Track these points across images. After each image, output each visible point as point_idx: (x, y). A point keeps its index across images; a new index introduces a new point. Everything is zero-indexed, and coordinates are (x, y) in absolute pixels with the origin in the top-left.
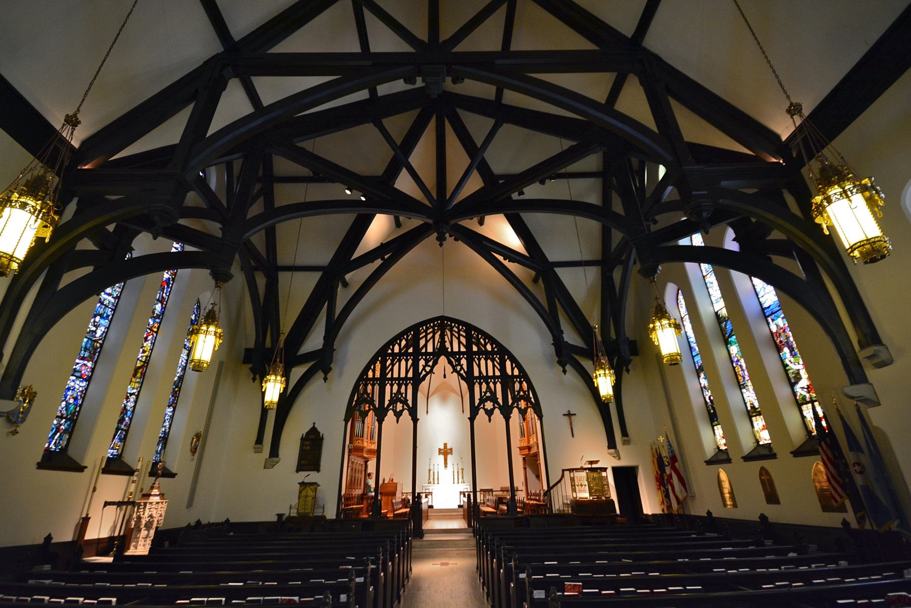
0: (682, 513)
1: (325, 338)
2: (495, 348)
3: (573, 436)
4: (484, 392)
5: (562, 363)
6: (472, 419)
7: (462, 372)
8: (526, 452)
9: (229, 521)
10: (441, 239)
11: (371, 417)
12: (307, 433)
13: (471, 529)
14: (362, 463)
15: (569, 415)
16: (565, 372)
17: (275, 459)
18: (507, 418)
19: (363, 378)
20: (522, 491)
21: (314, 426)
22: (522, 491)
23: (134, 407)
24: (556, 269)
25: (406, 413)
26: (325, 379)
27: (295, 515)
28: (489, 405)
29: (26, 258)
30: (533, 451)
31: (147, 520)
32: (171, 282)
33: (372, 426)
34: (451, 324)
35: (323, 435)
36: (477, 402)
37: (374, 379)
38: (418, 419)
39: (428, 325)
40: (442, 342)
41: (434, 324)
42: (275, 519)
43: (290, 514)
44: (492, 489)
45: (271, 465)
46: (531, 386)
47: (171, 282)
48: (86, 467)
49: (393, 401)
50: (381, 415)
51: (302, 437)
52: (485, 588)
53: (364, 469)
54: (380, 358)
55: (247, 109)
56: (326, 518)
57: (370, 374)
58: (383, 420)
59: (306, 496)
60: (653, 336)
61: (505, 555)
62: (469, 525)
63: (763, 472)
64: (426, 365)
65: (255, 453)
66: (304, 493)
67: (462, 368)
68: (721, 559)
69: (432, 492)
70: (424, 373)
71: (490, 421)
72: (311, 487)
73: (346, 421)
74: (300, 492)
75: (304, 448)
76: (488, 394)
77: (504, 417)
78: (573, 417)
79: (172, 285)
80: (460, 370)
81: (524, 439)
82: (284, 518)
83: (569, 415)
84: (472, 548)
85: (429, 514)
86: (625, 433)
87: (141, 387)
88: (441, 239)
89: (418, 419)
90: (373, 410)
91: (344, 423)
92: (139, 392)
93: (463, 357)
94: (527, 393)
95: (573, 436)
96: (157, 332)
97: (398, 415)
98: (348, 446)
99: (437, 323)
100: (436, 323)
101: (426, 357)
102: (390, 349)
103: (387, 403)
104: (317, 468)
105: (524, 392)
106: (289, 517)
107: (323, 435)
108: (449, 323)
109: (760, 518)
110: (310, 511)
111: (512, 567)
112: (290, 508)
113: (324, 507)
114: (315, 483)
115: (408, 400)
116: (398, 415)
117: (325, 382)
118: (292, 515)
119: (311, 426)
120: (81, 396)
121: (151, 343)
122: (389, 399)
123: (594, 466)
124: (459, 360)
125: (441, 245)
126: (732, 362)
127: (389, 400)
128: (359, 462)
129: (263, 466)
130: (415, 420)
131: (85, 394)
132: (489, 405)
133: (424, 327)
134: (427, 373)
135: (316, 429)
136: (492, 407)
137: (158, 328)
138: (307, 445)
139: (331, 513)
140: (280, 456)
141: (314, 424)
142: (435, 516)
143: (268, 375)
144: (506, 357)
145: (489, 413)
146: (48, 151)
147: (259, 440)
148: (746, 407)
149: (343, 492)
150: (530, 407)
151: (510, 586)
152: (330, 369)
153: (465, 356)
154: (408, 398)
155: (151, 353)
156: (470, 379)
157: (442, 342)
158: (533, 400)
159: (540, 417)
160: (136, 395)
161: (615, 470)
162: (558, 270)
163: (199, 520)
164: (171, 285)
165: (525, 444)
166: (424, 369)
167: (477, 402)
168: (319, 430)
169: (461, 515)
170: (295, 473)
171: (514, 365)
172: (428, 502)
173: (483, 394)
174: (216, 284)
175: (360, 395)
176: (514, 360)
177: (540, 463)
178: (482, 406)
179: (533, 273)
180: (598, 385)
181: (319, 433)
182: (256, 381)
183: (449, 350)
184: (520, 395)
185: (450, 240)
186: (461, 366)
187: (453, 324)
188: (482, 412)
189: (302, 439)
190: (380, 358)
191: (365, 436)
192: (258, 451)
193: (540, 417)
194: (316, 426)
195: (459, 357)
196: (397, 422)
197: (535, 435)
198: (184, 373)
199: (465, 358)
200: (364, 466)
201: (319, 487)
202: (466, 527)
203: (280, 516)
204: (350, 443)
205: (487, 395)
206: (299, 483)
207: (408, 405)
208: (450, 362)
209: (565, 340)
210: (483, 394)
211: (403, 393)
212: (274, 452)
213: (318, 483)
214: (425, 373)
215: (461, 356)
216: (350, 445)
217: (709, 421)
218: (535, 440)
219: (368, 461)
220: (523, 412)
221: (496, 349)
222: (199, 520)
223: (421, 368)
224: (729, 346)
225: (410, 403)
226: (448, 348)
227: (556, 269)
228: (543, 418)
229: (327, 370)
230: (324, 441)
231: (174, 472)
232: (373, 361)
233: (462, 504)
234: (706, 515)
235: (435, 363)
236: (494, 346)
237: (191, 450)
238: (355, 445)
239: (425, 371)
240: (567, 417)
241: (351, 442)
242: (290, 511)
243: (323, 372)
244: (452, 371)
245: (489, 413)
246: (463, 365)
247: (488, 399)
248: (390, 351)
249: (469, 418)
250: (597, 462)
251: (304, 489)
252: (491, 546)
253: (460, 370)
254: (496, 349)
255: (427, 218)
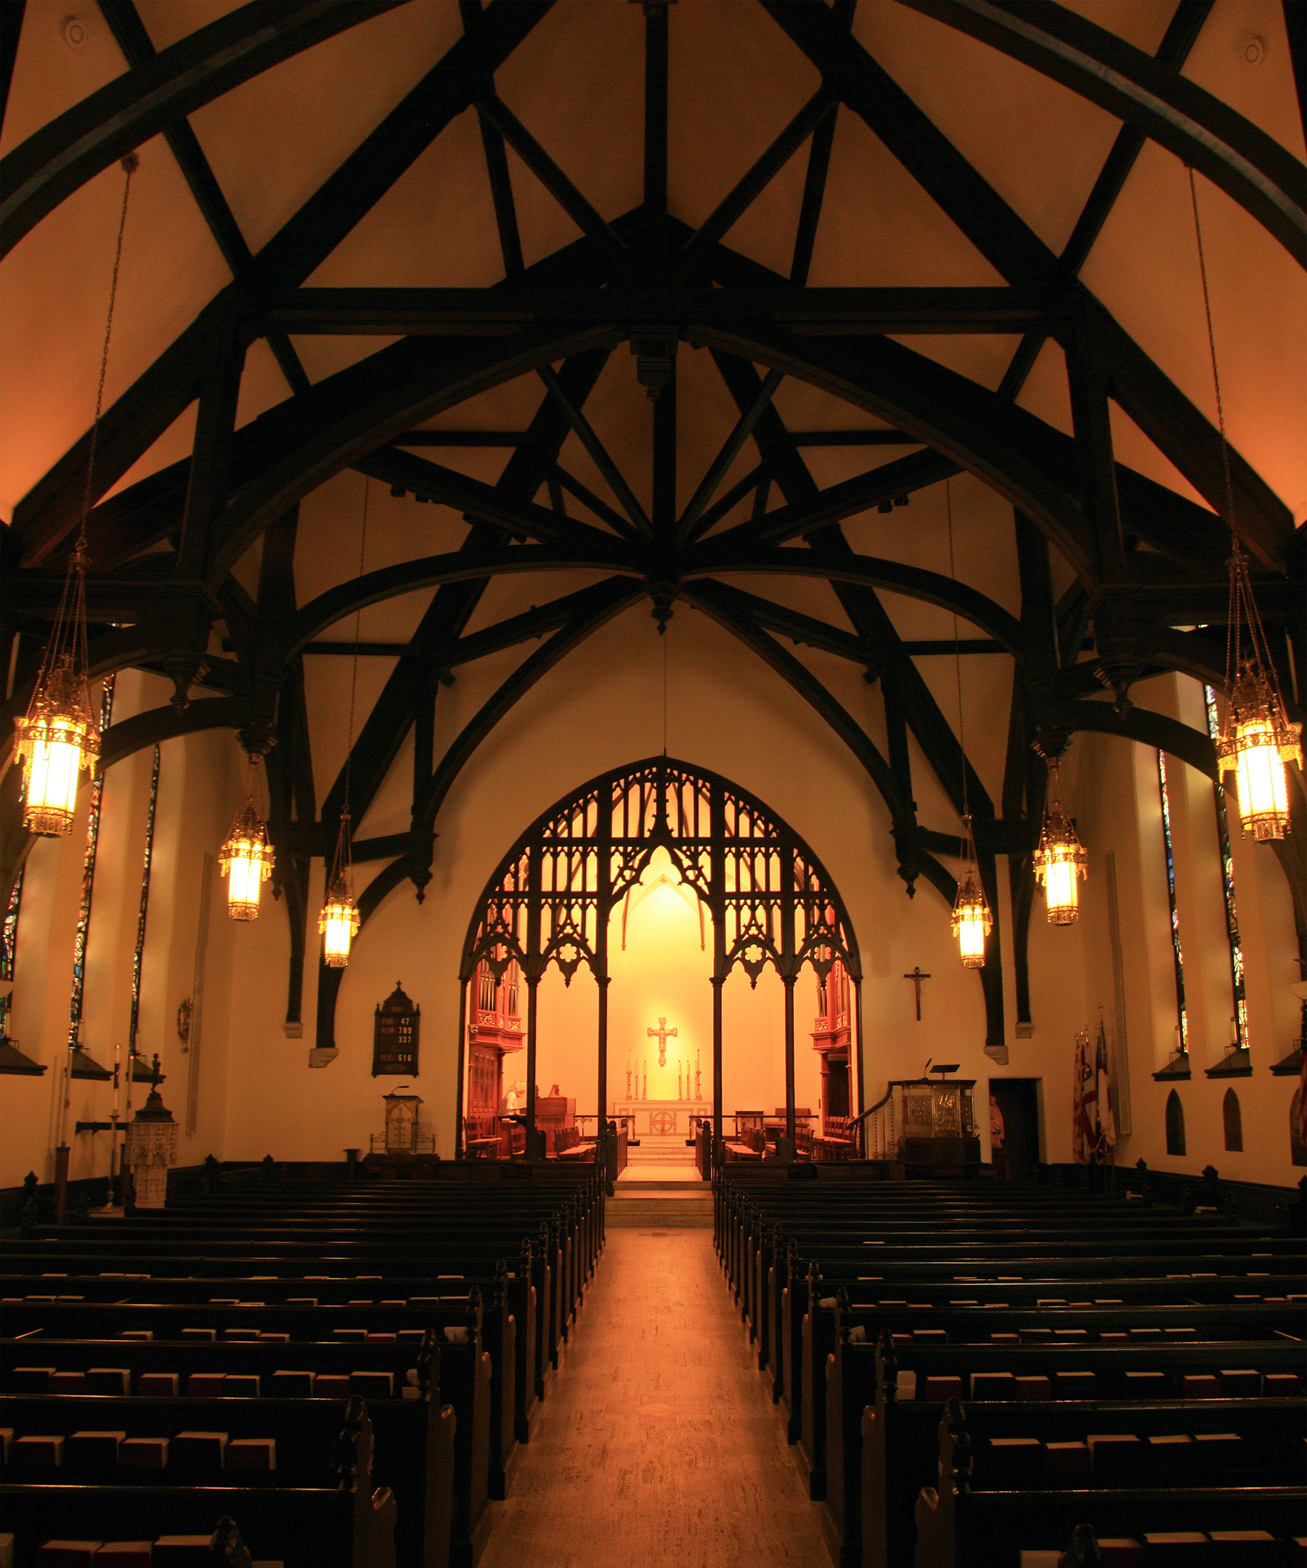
0: (1110, 1164)
1: (415, 810)
2: (773, 830)
3: (919, 1019)
4: (744, 926)
5: (908, 874)
6: (718, 981)
7: (701, 883)
8: (827, 1044)
9: (272, 1159)
10: (662, 614)
11: (516, 977)
12: (385, 1002)
13: (708, 1184)
14: (492, 1058)
15: (917, 976)
16: (911, 891)
17: (329, 1050)
18: (789, 981)
19: (493, 891)
20: (817, 1117)
21: (399, 989)
22: (817, 1117)
23: (83, 957)
24: (916, 660)
25: (584, 966)
26: (421, 897)
27: (383, 1152)
28: (754, 953)
29: (261, 902)
30: (841, 1043)
31: (155, 1152)
32: (109, 700)
33: (511, 985)
34: (680, 775)
35: (418, 1005)
36: (729, 946)
37: (516, 894)
38: (609, 980)
39: (631, 777)
40: (661, 816)
41: (642, 773)
42: (343, 1158)
43: (371, 1150)
44: (762, 1112)
45: (322, 1061)
46: (842, 915)
47: (109, 700)
48: (45, 1068)
49: (556, 942)
50: (534, 966)
51: (378, 1008)
52: (733, 1285)
53: (496, 1069)
54: (528, 850)
55: (281, 392)
56: (439, 1158)
57: (508, 883)
58: (539, 980)
59: (400, 1120)
60: (1038, 870)
61: (794, 1263)
62: (706, 1176)
63: (1174, 1100)
64: (626, 867)
65: (289, 1037)
66: (395, 1114)
67: (700, 874)
68: (1246, 1257)
69: (634, 1117)
70: (621, 883)
71: (753, 985)
72: (408, 1104)
73: (464, 979)
74: (389, 1112)
75: (383, 1030)
76: (753, 931)
77: (784, 979)
78: (924, 982)
79: (111, 705)
80: (697, 878)
81: (825, 1018)
82: (361, 1159)
83: (917, 976)
84: (709, 1213)
85: (629, 1157)
86: (1024, 1014)
87: (88, 917)
88: (662, 614)
89: (609, 980)
90: (518, 960)
91: (459, 982)
92: (87, 925)
93: (704, 850)
94: (833, 929)
95: (919, 1019)
96: (99, 808)
97: (568, 969)
98: (469, 1026)
99: (651, 772)
100: (647, 772)
101: (625, 849)
102: (549, 829)
103: (544, 944)
104: (412, 1069)
105: (828, 928)
106: (371, 1156)
107: (418, 1005)
108: (676, 773)
109: (1204, 1172)
110: (409, 1146)
111: (807, 1286)
112: (372, 1140)
113: (434, 1140)
114: (415, 1098)
115: (587, 940)
116: (568, 969)
117: (421, 903)
118: (375, 1152)
119: (394, 988)
120: (9, 944)
121: (93, 831)
122: (550, 936)
123: (950, 1076)
124: (694, 857)
125: (662, 629)
126: (1225, 888)
127: (548, 940)
128: (487, 1057)
129: (307, 1063)
130: (603, 981)
131: (15, 940)
132: (754, 953)
133: (622, 782)
134: (629, 884)
135: (404, 994)
136: (760, 958)
137: (100, 799)
138: (388, 1026)
139: (447, 1152)
140: (337, 1046)
141: (399, 983)
142: (640, 1159)
143: (231, 838)
144: (795, 852)
145: (753, 970)
146: (337, 849)
147: (294, 1014)
148: (1234, 981)
149: (465, 1114)
150: (838, 958)
151: (825, 1359)
152: (430, 876)
153: (708, 848)
154: (587, 936)
155: (95, 850)
156: (715, 897)
157: (661, 816)
158: (845, 944)
159: (857, 980)
160: (83, 932)
161: (997, 1086)
162: (922, 664)
163: (211, 1156)
164: (108, 707)
165: (825, 1029)
166: (621, 874)
167: (729, 946)
168: (409, 995)
169: (692, 1159)
170: (372, 1077)
171: (811, 870)
172: (626, 1134)
173: (743, 930)
174: (250, 758)
175: (489, 928)
176: (810, 857)
177: (851, 1068)
178: (739, 955)
179: (864, 669)
180: (958, 935)
181: (411, 1002)
182: (280, 897)
183: (675, 834)
184: (819, 934)
185: (681, 608)
186: (700, 869)
187: (684, 776)
188: (738, 967)
189: (378, 1014)
190: (528, 850)
191: (500, 1008)
192: (295, 1034)
193: (857, 980)
194: (403, 989)
195: (696, 849)
196: (568, 984)
197: (846, 1012)
198: (148, 883)
199: (708, 853)
200: (496, 1064)
201: (422, 1104)
202: (700, 1178)
203: (352, 1153)
204: (471, 1023)
205: (751, 932)
206: (384, 1097)
207: (587, 950)
208: (676, 861)
209: (919, 824)
210: (743, 930)
211: (577, 925)
212: (326, 1037)
213: (421, 1097)
214: (624, 883)
215: (700, 848)
216: (472, 1026)
217: (1176, 1001)
218: (845, 1023)
219: (504, 1054)
220: (823, 969)
221: (774, 835)
222: (211, 1156)
223: (614, 872)
224: (1225, 857)
225: (592, 944)
226: (672, 830)
227: (916, 660)
228: (863, 982)
229: (422, 879)
230: (421, 1017)
231: (41, 1063)
232: (514, 856)
233: (694, 1138)
234: (1136, 1167)
235: (645, 862)
236: (771, 827)
237: (180, 1033)
238: (482, 1024)
239: (624, 879)
240: (911, 982)
241: (473, 1020)
242: (372, 1145)
243: (414, 881)
244: (680, 880)
245: (753, 970)
246: (702, 867)
247: (754, 940)
248: (548, 834)
249: (711, 980)
250: (953, 1068)
251: (394, 1107)
252: (794, 1276)
253: (697, 878)
254: (774, 835)
255: (634, 571)
